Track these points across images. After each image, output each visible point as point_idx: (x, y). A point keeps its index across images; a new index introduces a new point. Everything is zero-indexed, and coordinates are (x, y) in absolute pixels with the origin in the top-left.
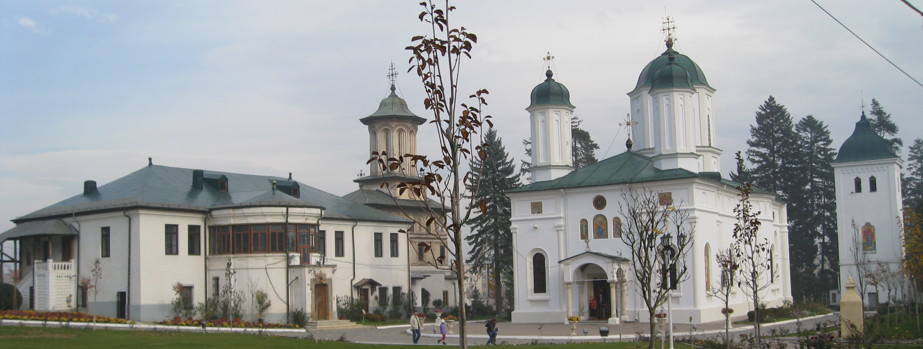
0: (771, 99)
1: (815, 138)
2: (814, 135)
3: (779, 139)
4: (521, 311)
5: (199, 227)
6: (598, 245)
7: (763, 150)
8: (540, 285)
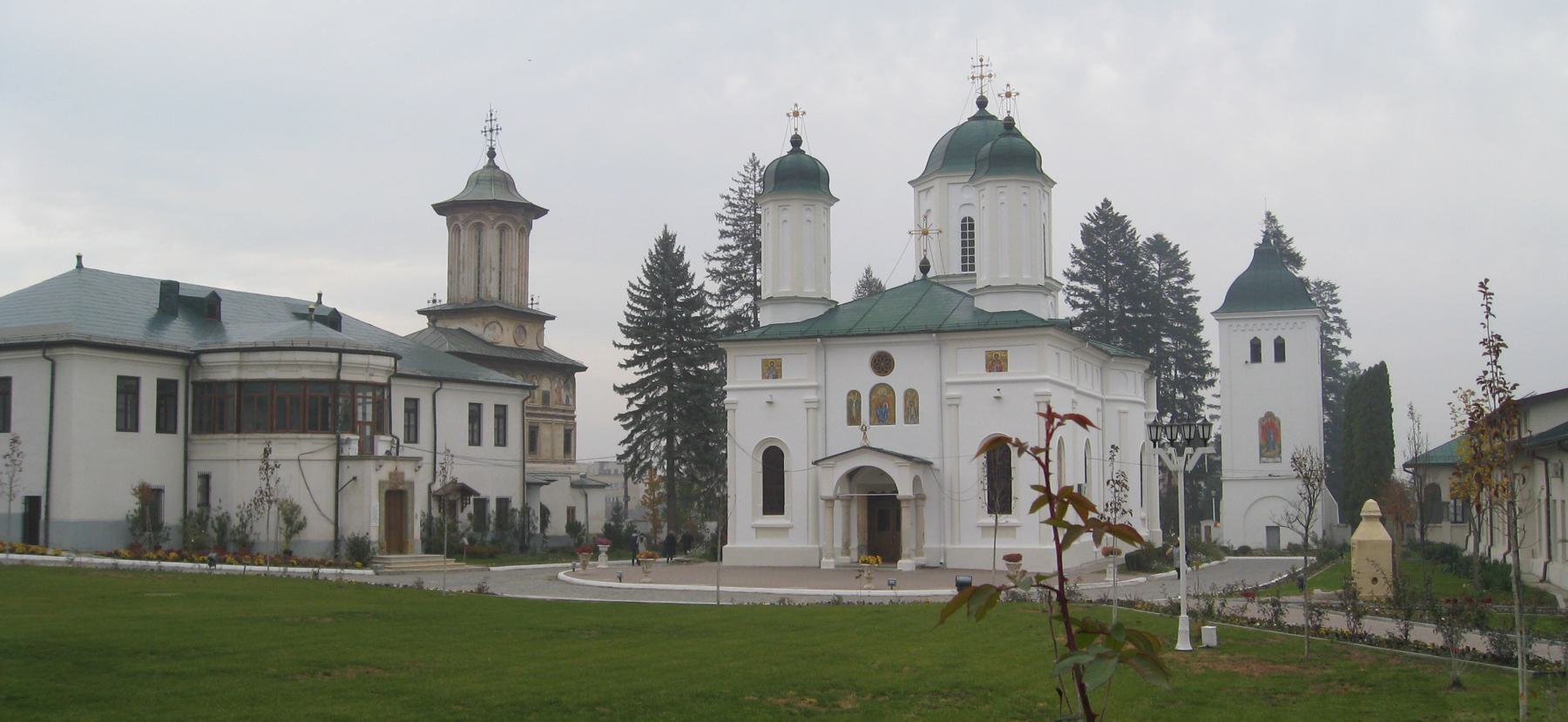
0: (1106, 203)
1: (1167, 270)
2: (1164, 265)
3: (1117, 270)
4: (739, 545)
5: (175, 382)
6: (880, 436)
7: (1092, 288)
8: (774, 501)
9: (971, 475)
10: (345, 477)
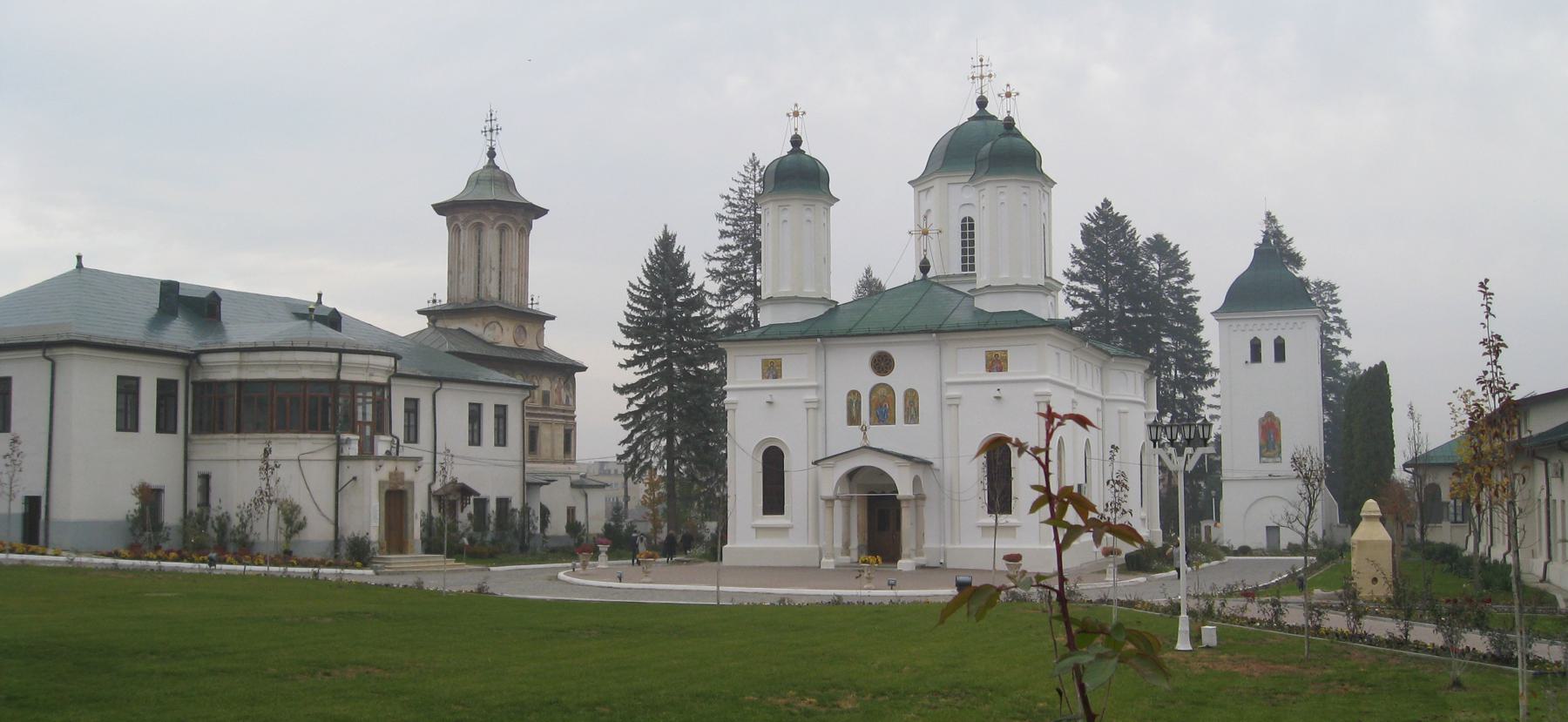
0: (1106, 203)
1: (1167, 270)
2: (1164, 265)
3: (1117, 270)
4: (739, 545)
5: (175, 382)
6: (880, 436)
7: (1092, 288)
8: (774, 501)
9: (971, 475)
10: (345, 477)
